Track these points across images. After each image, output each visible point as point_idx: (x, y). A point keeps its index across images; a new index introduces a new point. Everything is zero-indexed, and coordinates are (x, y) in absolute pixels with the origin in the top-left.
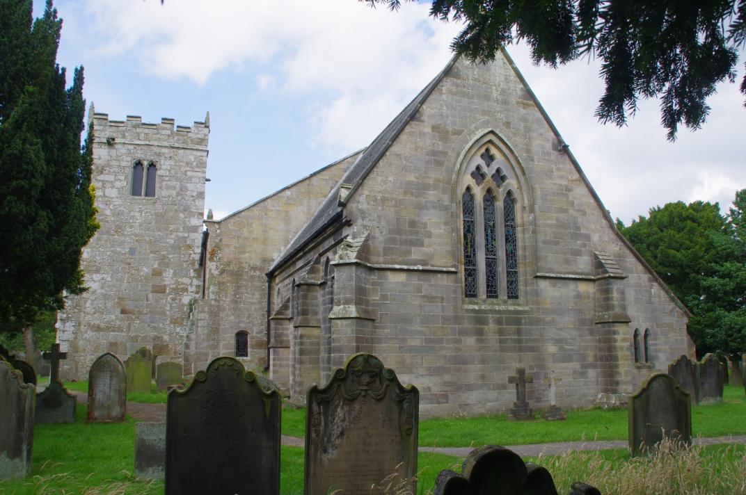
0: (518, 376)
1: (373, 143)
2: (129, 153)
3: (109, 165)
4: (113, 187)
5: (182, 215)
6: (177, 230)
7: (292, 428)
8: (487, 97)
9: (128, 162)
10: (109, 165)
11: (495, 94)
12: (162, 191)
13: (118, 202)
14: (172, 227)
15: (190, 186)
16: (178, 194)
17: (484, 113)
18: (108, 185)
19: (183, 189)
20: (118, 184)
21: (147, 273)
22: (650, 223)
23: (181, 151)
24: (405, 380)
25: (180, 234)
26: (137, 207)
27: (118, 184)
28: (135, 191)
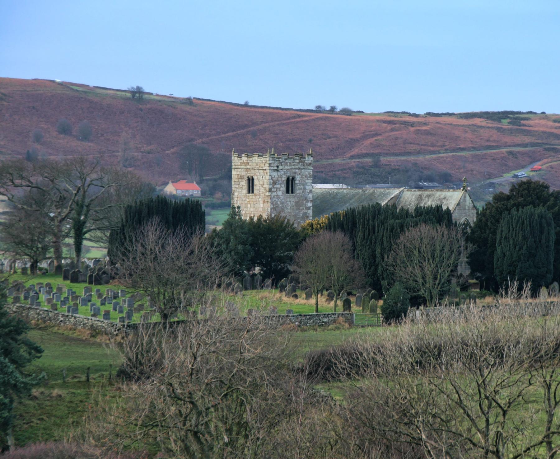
0: (24, 285)
1: (277, 108)
2: (285, 174)
3: (278, 180)
4: (280, 190)
5: (304, 202)
6: (303, 209)
7: (427, 260)
8: (465, 209)
9: (284, 179)
10: (278, 180)
11: (467, 208)
12: (298, 192)
13: (282, 197)
14: (301, 208)
15: (307, 187)
16: (303, 192)
17: (464, 213)
18: (278, 190)
19: (305, 189)
20: (282, 189)
21: (246, 220)
22: (452, 188)
23: (303, 170)
24: (68, 282)
25: (305, 211)
26: (288, 200)
27: (282, 189)
28: (288, 192)
